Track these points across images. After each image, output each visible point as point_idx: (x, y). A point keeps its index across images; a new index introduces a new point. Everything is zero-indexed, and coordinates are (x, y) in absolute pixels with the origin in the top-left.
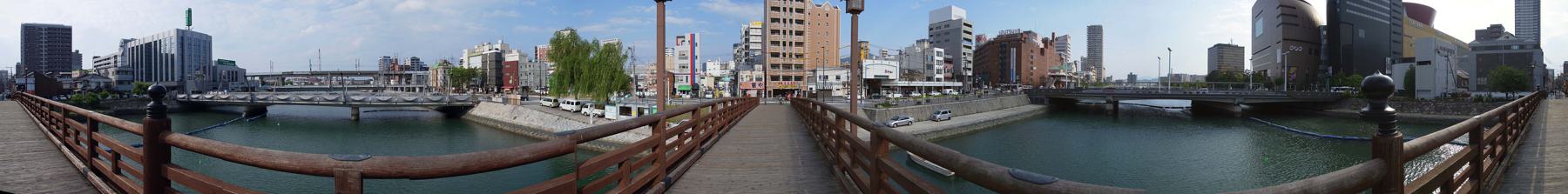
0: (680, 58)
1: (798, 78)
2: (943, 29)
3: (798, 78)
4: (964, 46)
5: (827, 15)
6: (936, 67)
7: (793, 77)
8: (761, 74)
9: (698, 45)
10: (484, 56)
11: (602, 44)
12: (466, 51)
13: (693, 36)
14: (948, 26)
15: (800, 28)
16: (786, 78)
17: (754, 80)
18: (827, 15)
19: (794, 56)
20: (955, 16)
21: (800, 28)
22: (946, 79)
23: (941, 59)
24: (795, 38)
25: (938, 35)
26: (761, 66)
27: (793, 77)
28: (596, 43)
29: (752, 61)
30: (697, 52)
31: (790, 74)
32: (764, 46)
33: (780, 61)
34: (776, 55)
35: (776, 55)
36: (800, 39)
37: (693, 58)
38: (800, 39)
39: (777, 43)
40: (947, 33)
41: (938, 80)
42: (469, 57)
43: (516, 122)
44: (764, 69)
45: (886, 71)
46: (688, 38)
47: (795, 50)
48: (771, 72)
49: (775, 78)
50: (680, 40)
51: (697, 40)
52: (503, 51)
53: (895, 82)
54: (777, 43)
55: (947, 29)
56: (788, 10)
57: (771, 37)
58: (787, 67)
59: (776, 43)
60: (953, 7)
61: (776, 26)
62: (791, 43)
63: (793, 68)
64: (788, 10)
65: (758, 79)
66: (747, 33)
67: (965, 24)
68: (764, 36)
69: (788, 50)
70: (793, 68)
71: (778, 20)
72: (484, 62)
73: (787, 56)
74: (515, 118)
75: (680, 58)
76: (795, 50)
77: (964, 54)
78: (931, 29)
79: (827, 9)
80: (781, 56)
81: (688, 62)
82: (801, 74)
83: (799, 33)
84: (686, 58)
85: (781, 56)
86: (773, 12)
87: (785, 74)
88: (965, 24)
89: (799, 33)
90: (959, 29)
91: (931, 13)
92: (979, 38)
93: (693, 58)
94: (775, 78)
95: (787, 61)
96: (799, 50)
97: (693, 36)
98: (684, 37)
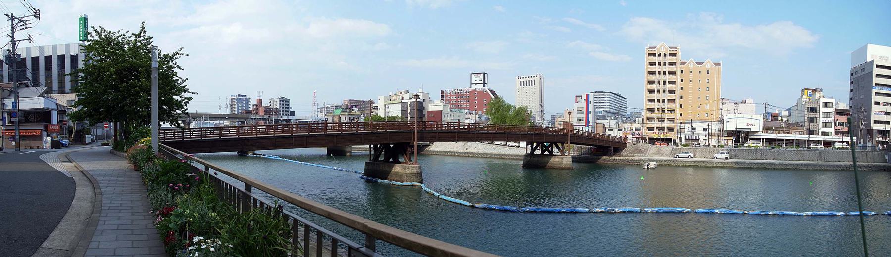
0: (578, 113)
1: (671, 130)
3: (671, 130)
4: (876, 94)
5: (708, 73)
6: (822, 119)
7: (655, 128)
10: (405, 105)
11: (517, 108)
12: (382, 98)
16: (659, 129)
17: (634, 130)
18: (708, 73)
22: (837, 133)
27: (655, 128)
28: (515, 107)
30: (591, 109)
37: (588, 112)
41: (824, 134)
42: (385, 105)
43: (468, 151)
45: (748, 124)
46: (584, 97)
49: (651, 129)
51: (591, 99)
52: (424, 100)
53: (759, 134)
56: (662, 73)
58: (661, 120)
65: (636, 130)
67: (878, 66)
72: (404, 111)
74: (467, 149)
75: (578, 113)
76: (667, 106)
77: (877, 103)
78: (852, 74)
79: (708, 67)
81: (583, 116)
82: (672, 126)
84: (582, 113)
86: (671, 57)
87: (659, 125)
88: (878, 66)
90: (871, 73)
93: (588, 112)
94: (651, 129)
97: (587, 96)
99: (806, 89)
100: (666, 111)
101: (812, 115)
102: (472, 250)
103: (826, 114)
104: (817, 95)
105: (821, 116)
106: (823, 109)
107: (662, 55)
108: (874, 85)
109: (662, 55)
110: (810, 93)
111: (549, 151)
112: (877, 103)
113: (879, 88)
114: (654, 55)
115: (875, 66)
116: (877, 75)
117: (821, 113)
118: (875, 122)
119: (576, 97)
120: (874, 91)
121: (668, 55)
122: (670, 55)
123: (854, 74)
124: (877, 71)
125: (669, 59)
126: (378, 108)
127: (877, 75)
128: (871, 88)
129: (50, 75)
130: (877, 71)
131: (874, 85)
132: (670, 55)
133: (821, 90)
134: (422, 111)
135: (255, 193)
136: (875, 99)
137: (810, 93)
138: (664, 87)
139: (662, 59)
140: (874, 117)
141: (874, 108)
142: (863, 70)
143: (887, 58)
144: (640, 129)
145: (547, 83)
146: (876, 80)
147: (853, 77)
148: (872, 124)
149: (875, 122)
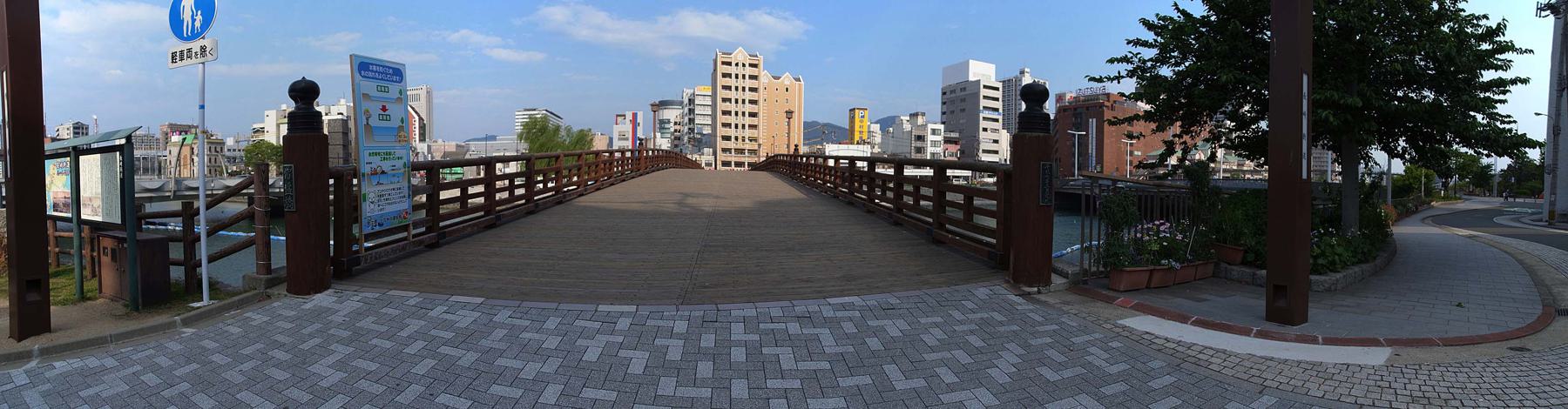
0: (619, 139)
2: (959, 93)
4: (984, 118)
5: (787, 90)
7: (733, 163)
8: (711, 158)
9: (641, 124)
13: (635, 115)
14: (965, 89)
15: (754, 108)
18: (787, 90)
19: (747, 141)
20: (974, 74)
21: (754, 108)
23: (939, 138)
24: (748, 121)
25: (953, 102)
26: (711, 150)
27: (733, 163)
29: (699, 141)
31: (742, 160)
32: (714, 106)
33: (731, 145)
34: (727, 138)
35: (727, 138)
36: (754, 121)
38: (754, 121)
39: (729, 88)
40: (963, 100)
44: (715, 154)
46: (629, 116)
47: (748, 133)
48: (721, 157)
50: (620, 119)
51: (640, 119)
54: (729, 88)
55: (963, 93)
56: (740, 89)
57: (721, 93)
58: (740, 151)
59: (728, 88)
60: (971, 61)
61: (726, 132)
62: (743, 126)
63: (747, 154)
64: (740, 89)
66: (691, 101)
67: (985, 87)
68: (714, 106)
69: (740, 133)
70: (747, 154)
71: (730, 100)
73: (740, 140)
76: (748, 133)
77: (985, 130)
78: (944, 94)
79: (787, 83)
80: (733, 139)
83: (753, 115)
84: (627, 139)
85: (733, 139)
86: (725, 66)
87: (737, 160)
88: (985, 87)
89: (753, 115)
90: (978, 94)
91: (945, 70)
92: (1060, 98)
95: (740, 145)
96: (754, 133)
97: (635, 115)
98: (624, 116)
100: (747, 141)
101: (919, 144)
102: (1178, 323)
103: (934, 143)
104: (920, 120)
105: (929, 145)
106: (930, 137)
107: (740, 65)
108: (981, 108)
109: (740, 65)
112: (985, 130)
114: (729, 64)
115: (982, 87)
116: (997, 99)
117: (929, 142)
118: (984, 151)
119: (618, 116)
120: (981, 115)
121: (747, 65)
122: (751, 65)
124: (984, 92)
126: (266, 130)
128: (978, 112)
130: (984, 92)
131: (981, 108)
132: (751, 65)
133: (923, 114)
134: (347, 134)
136: (983, 124)
138: (744, 107)
139: (740, 71)
140: (983, 146)
141: (982, 135)
142: (964, 89)
144: (70, 152)
145: (435, 94)
146: (984, 102)
147: (945, 96)
148: (980, 154)
149: (984, 151)
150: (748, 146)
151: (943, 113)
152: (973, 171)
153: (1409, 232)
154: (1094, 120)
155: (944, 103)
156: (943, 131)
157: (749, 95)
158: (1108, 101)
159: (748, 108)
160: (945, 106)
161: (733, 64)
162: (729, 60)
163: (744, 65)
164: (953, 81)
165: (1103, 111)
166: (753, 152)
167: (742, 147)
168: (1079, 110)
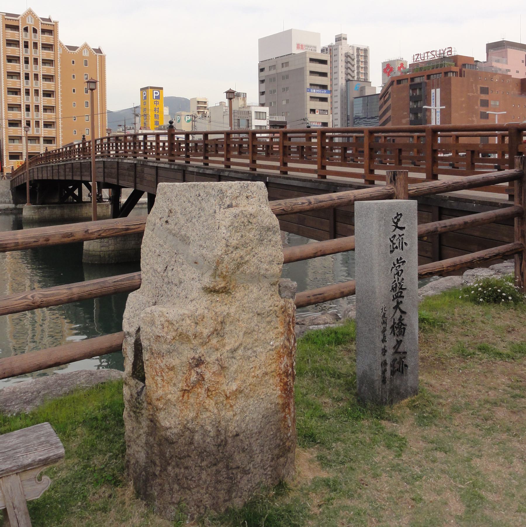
2: (280, 70)
15: (49, 86)
25: (272, 79)
55: (285, 69)
71: (19, 107)
77: (313, 111)
78: (262, 70)
83: (48, 94)
88: (312, 60)
90: (301, 70)
91: (264, 43)
99: (151, 88)
107: (30, 30)
108: (308, 86)
109: (30, 30)
110: (156, 93)
111: (74, 189)
112: (313, 111)
113: (314, 91)
114: (16, 28)
123: (267, 69)
125: (41, 38)
127: (312, 73)
129: (424, 220)
132: (44, 31)
135: (21, 387)
137: (156, 93)
138: (35, 37)
139: (30, 37)
142: (285, 64)
143: (315, 47)
147: (263, 73)
150: (43, 132)
151: (262, 93)
152: (508, 144)
153: (475, 195)
154: (438, 90)
155: (262, 81)
156: (268, 115)
157: (42, 70)
158: (456, 65)
159: (42, 85)
160: (264, 85)
161: (21, 29)
162: (15, 24)
163: (35, 31)
164: (272, 55)
165: (450, 78)
166: (49, 140)
167: (35, 134)
168: (417, 80)
